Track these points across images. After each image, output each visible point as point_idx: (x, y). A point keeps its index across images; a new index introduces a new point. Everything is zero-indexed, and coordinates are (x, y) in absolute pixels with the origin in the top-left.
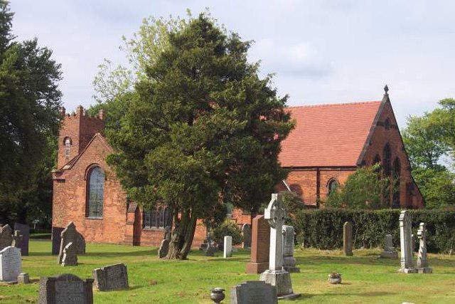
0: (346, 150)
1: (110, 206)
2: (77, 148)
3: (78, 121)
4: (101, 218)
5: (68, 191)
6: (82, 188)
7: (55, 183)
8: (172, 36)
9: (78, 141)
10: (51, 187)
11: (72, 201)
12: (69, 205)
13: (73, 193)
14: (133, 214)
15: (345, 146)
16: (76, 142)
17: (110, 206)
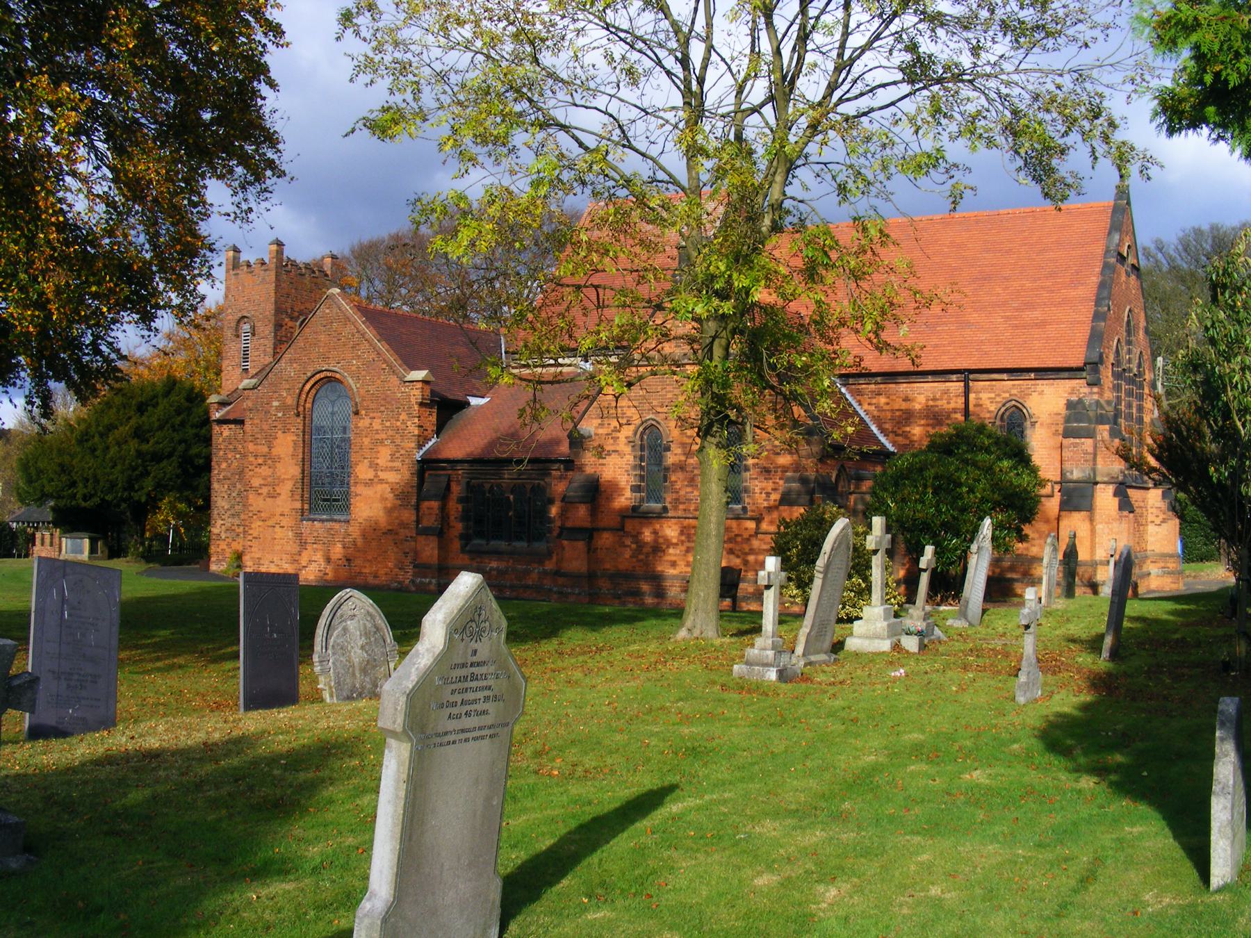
0: (1042, 324)
1: (369, 483)
2: (269, 343)
3: (271, 276)
4: (343, 518)
5: (251, 447)
6: (290, 438)
7: (216, 428)
8: (1060, 738)
9: (271, 328)
10: (208, 441)
11: (265, 471)
12: (256, 482)
13: (265, 449)
14: (435, 504)
15: (1037, 314)
16: (266, 330)
17: (369, 483)
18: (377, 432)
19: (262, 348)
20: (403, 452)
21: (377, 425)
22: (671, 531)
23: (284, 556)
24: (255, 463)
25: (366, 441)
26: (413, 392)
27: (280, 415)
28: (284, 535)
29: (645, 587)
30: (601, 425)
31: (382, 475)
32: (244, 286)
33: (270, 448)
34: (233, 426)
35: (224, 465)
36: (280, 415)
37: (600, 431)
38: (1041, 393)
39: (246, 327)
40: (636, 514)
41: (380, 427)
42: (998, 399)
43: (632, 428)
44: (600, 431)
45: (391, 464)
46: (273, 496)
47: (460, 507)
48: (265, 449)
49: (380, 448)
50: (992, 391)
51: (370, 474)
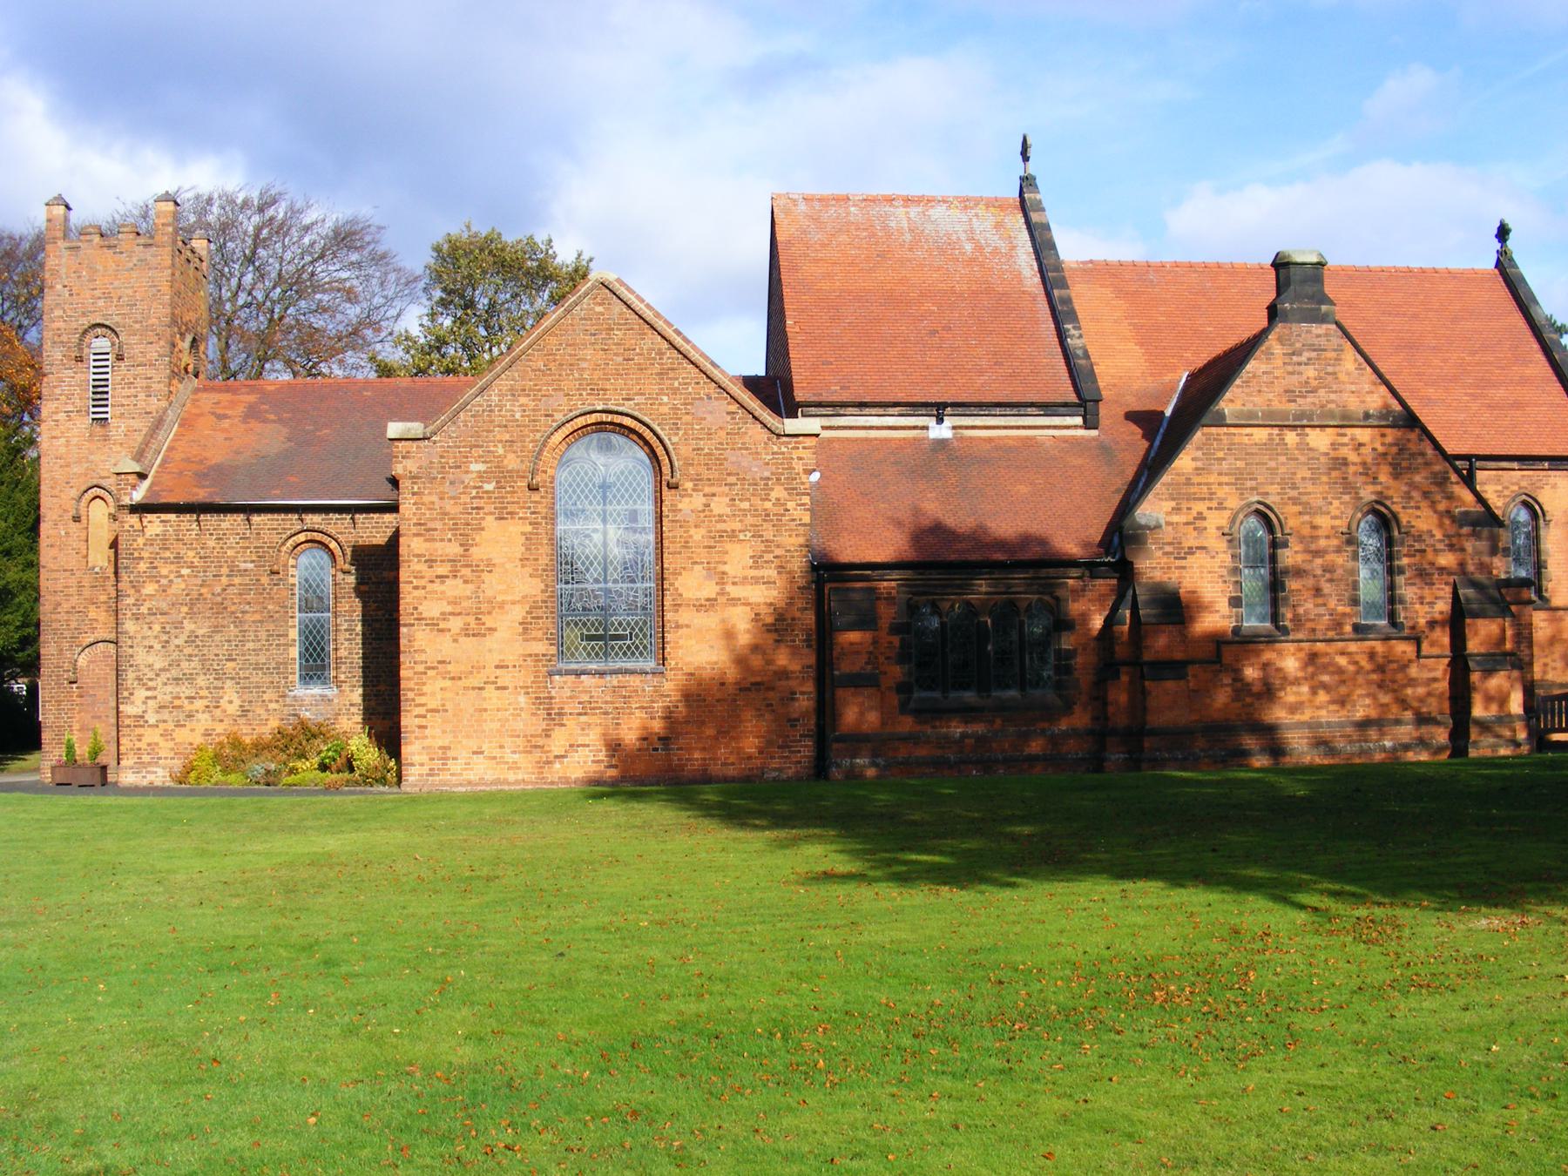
11: (454, 588)
13: (454, 549)
18: (721, 519)
19: (140, 383)
20: (778, 552)
21: (720, 506)
22: (1290, 663)
23: (508, 741)
24: (429, 573)
25: (697, 535)
26: (801, 452)
27: (489, 487)
28: (511, 707)
29: (1250, 742)
30: (1177, 510)
31: (734, 591)
32: (92, 270)
33: (466, 547)
34: (172, 517)
35: (150, 589)
36: (489, 487)
37: (1175, 518)
38: (1554, 486)
39: (102, 344)
40: (1240, 643)
41: (728, 511)
42: (1506, 493)
43: (1227, 514)
44: (1175, 518)
45: (753, 573)
46: (477, 631)
47: (896, 640)
48: (454, 549)
49: (729, 546)
50: (1498, 481)
51: (710, 590)
